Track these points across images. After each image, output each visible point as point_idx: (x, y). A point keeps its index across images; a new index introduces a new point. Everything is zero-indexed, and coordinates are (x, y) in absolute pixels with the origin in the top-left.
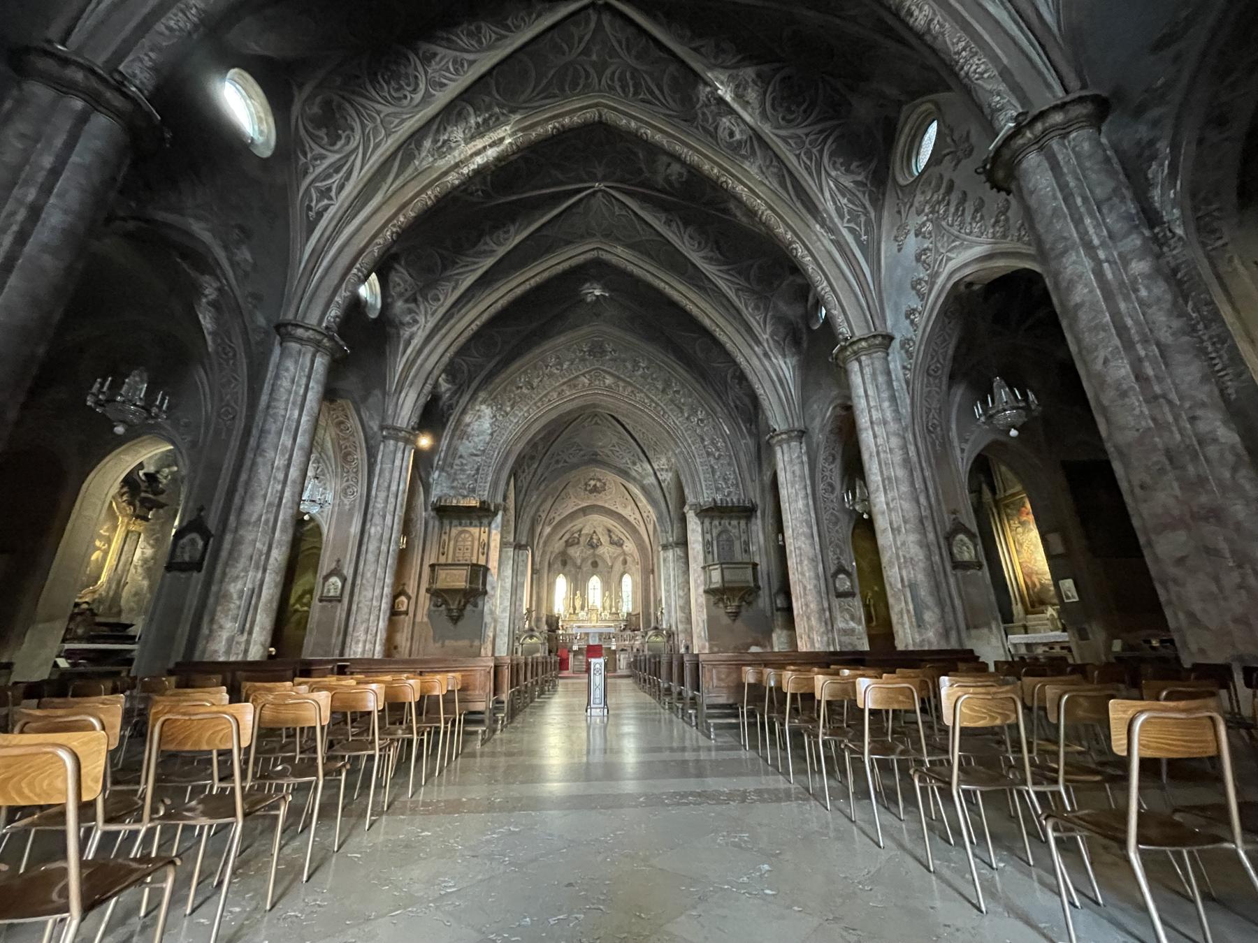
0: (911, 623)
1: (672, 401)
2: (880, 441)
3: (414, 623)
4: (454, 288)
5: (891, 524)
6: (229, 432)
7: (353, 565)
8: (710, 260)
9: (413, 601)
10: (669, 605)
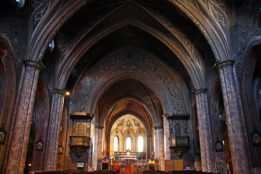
0: (238, 164)
1: (158, 74)
2: (230, 99)
3: (65, 156)
4: (78, 39)
5: (233, 129)
6: (11, 98)
7: (46, 138)
8: (171, 27)
9: (64, 149)
10: (156, 150)
